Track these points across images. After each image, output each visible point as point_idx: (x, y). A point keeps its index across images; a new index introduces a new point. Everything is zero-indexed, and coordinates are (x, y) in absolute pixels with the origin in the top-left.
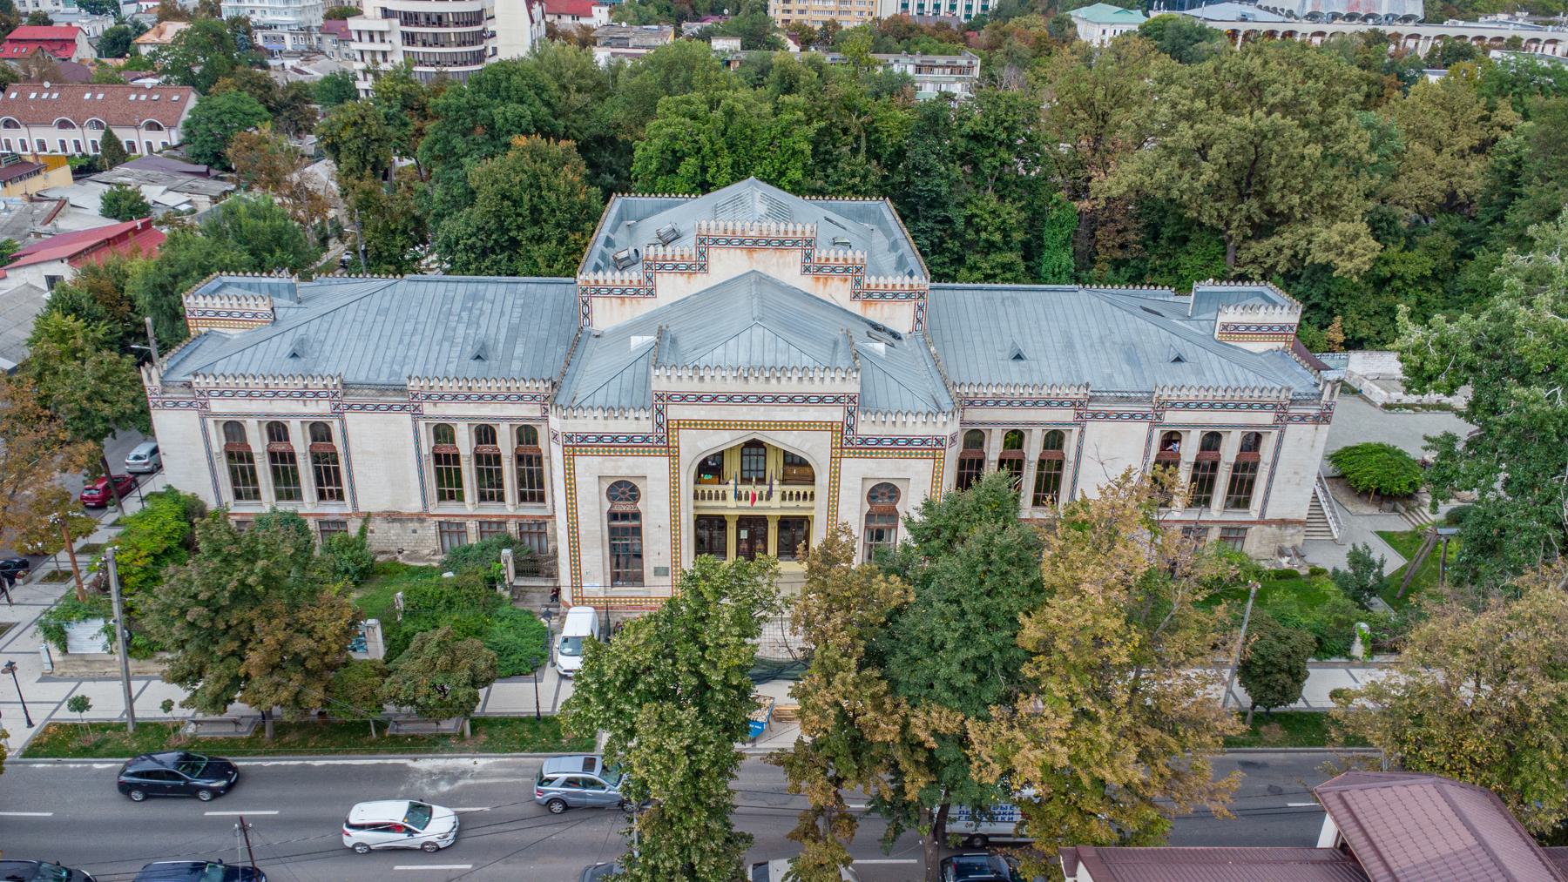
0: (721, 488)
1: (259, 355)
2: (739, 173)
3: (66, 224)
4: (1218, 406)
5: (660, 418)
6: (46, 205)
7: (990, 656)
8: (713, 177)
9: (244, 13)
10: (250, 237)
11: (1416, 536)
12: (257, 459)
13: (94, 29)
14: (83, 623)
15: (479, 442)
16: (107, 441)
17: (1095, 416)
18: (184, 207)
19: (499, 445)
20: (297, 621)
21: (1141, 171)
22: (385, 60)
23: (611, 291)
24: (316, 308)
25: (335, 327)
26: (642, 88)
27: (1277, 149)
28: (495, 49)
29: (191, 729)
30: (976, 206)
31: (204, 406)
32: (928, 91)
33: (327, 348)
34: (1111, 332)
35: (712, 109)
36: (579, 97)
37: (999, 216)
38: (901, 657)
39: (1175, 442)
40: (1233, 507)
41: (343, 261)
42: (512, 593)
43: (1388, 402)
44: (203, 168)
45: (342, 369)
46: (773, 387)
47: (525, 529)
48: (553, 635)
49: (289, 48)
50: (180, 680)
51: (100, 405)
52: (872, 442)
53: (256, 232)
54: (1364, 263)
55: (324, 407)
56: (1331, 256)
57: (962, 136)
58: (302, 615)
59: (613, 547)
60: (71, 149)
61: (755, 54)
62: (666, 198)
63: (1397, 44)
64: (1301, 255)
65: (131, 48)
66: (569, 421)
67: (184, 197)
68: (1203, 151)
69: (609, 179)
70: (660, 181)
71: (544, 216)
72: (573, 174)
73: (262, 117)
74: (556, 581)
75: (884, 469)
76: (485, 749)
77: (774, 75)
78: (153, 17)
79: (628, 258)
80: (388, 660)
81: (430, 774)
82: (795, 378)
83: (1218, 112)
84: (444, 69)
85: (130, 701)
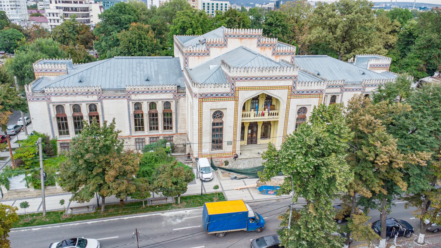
14: (16, 177)
17: (346, 90)
23: (195, 54)
29: (69, 211)
31: (49, 99)
46: (271, 74)
52: (301, 92)
55: (95, 98)
66: (202, 89)
68: (336, 27)
76: (188, 206)
81: (171, 217)
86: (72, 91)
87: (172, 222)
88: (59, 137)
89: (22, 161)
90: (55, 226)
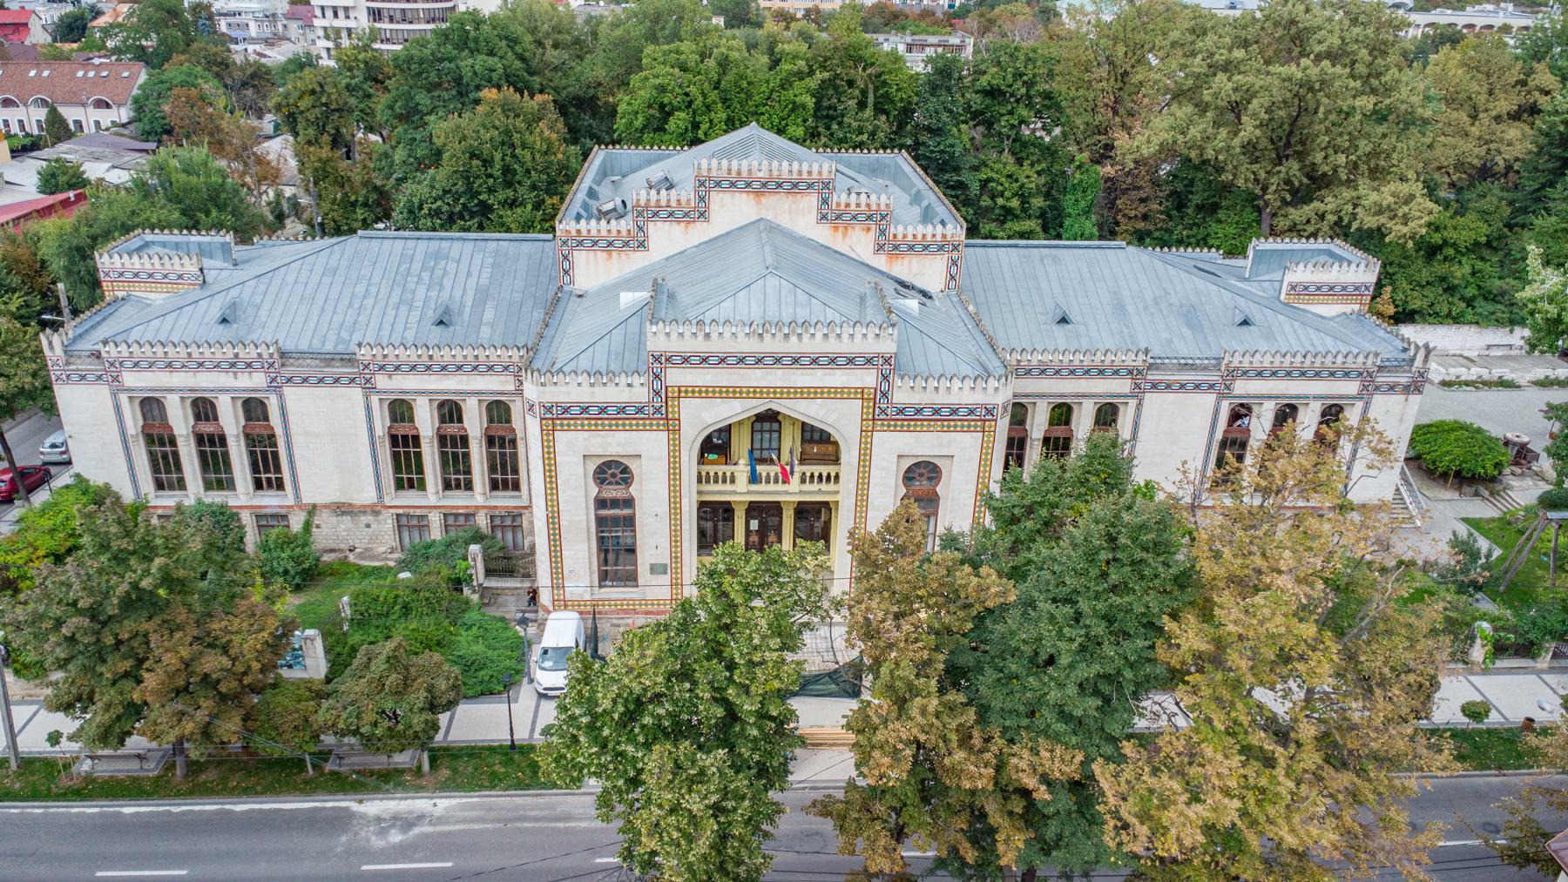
0: (728, 469)
1: (183, 321)
4: (1296, 374)
5: (657, 385)
7: (1119, 673)
11: (1505, 523)
12: (180, 442)
13: (52, 17)
15: (442, 421)
17: (1154, 386)
19: (466, 423)
20: (208, 634)
23: (595, 243)
25: (274, 288)
27: (1325, 101)
29: (86, 766)
30: (992, 169)
31: (116, 379)
33: (263, 313)
37: (1017, 181)
38: (990, 675)
42: (482, 597)
43: (1447, 379)
46: (793, 346)
47: (497, 522)
48: (530, 645)
50: (67, 707)
52: (910, 412)
53: (187, 190)
54: (1420, 226)
56: (1383, 219)
57: (977, 92)
58: (215, 626)
59: (601, 541)
62: (655, 151)
66: (549, 389)
68: (1236, 109)
72: (550, 130)
75: (924, 445)
76: (452, 785)
79: (614, 210)
80: (328, 680)
81: (379, 819)
82: (819, 335)
85: (12, 735)
86: (183, 354)
87: (374, 838)
88: (157, 497)
89: (8, 579)
90: (29, 810)
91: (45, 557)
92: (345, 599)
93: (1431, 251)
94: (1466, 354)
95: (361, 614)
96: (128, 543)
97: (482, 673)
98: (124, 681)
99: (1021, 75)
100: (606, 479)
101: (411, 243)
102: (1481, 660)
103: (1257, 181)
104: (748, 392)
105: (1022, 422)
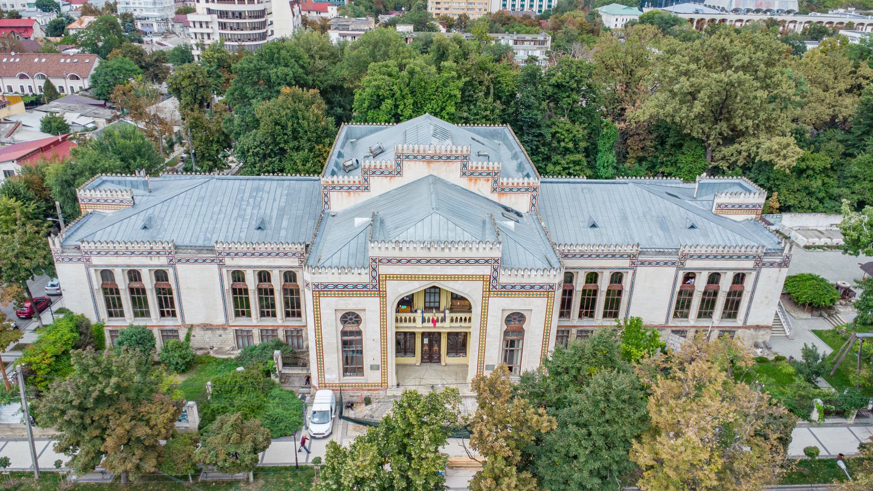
0: (412, 315)
1: (123, 228)
2: (418, 110)
3: (19, 137)
4: (719, 257)
5: (374, 274)
6: (8, 125)
8: (402, 111)
9: (129, 11)
10: (121, 150)
11: (836, 333)
13: (45, 20)
14: (7, 405)
16: (29, 282)
17: (642, 263)
18: (91, 126)
19: (273, 283)
21: (657, 106)
22: (209, 38)
23: (342, 188)
24: (159, 196)
26: (358, 57)
27: (741, 93)
28: (272, 31)
30: (558, 126)
31: (88, 260)
32: (521, 55)
33: (166, 222)
34: (650, 209)
35: (401, 70)
36: (321, 62)
39: (692, 278)
40: (726, 318)
41: (182, 158)
42: (281, 379)
43: (808, 244)
44: (102, 102)
45: (174, 237)
46: (446, 254)
49: (156, 31)
50: (65, 450)
51: (23, 260)
52: (509, 287)
53: (125, 147)
56: (773, 157)
57: (550, 85)
60: (27, 91)
61: (421, 34)
62: (375, 126)
63: (784, 26)
64: (753, 156)
65: (65, 31)
66: (316, 276)
67: (91, 120)
68: (693, 96)
69: (339, 111)
70: (370, 113)
71: (300, 135)
72: (318, 108)
73: (136, 72)
74: (308, 370)
75: (515, 304)
77: (433, 47)
78: (79, 13)
79: (352, 165)
82: (460, 248)
83: (704, 71)
84: (243, 43)
85: (35, 458)
89: (32, 370)
91: (51, 357)
92: (209, 383)
93: (800, 172)
94: (819, 229)
95: (217, 391)
96: (98, 369)
97: (281, 424)
98: (95, 440)
99: (574, 77)
100: (347, 321)
101: (243, 182)
102: (817, 420)
103: (704, 133)
104: (423, 278)
105: (571, 281)
